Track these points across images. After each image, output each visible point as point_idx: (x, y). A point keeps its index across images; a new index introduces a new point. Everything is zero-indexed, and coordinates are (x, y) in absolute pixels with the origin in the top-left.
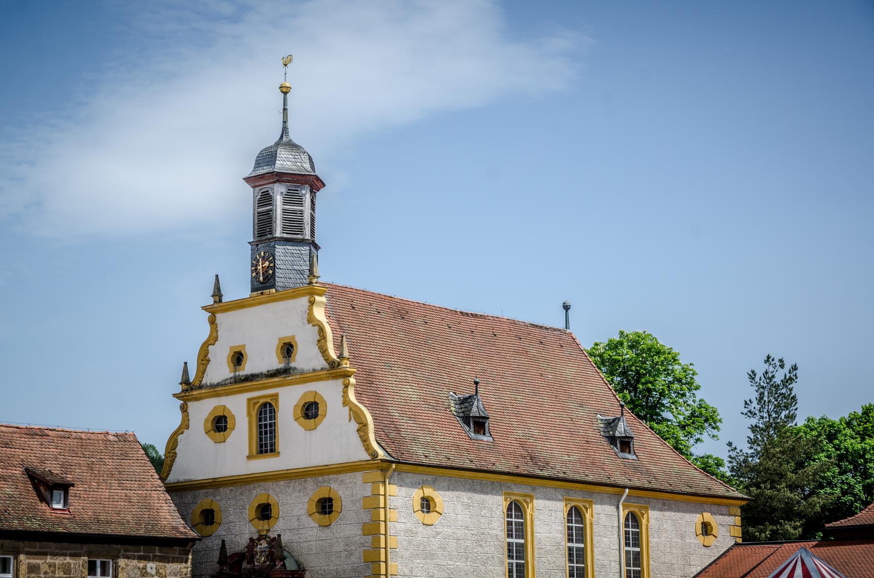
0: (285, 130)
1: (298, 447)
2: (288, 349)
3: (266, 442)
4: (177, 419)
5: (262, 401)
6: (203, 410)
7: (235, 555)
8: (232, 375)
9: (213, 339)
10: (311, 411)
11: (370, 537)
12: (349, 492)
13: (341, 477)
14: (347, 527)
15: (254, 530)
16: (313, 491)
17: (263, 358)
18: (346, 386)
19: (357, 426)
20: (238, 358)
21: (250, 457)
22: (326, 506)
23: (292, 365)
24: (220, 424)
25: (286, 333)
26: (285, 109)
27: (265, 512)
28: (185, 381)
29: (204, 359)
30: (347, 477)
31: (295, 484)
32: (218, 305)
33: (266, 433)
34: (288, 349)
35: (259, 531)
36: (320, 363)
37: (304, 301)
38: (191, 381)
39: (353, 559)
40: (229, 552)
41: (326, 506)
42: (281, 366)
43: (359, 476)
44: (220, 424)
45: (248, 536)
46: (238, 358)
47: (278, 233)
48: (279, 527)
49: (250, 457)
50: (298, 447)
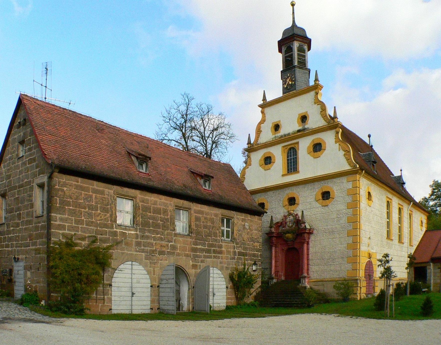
0: (294, 21)
1: (309, 166)
2: (304, 118)
3: (292, 166)
4: (259, 117)
5: (289, 147)
6: (258, 156)
7: (278, 223)
8: (274, 136)
9: (263, 121)
10: (317, 148)
11: (351, 209)
12: (338, 188)
13: (334, 180)
14: (339, 204)
15: (286, 211)
16: (318, 189)
17: (290, 126)
18: (337, 133)
19: (344, 153)
20: (277, 127)
21: (283, 175)
22: (326, 195)
23: (306, 126)
24: (268, 160)
25: (302, 111)
26: (293, 13)
27: (292, 201)
28: (249, 143)
29: (259, 131)
30: (337, 180)
31: (310, 186)
32: (265, 105)
33: (291, 163)
34: (304, 118)
35: (288, 212)
36: (322, 123)
37: (313, 93)
38: (252, 143)
39: (341, 222)
40: (274, 222)
41: (326, 195)
42: (301, 128)
43: (344, 179)
44: (268, 160)
45: (282, 214)
46: (277, 127)
47: (296, 64)
48: (298, 210)
49: (283, 175)
50: (309, 166)
